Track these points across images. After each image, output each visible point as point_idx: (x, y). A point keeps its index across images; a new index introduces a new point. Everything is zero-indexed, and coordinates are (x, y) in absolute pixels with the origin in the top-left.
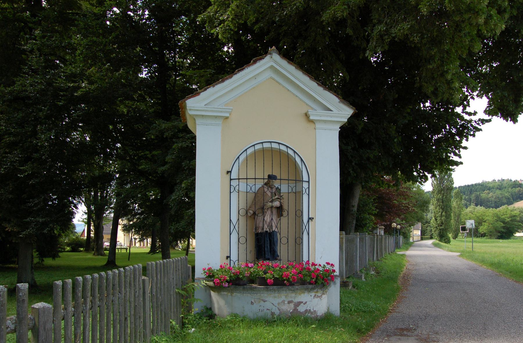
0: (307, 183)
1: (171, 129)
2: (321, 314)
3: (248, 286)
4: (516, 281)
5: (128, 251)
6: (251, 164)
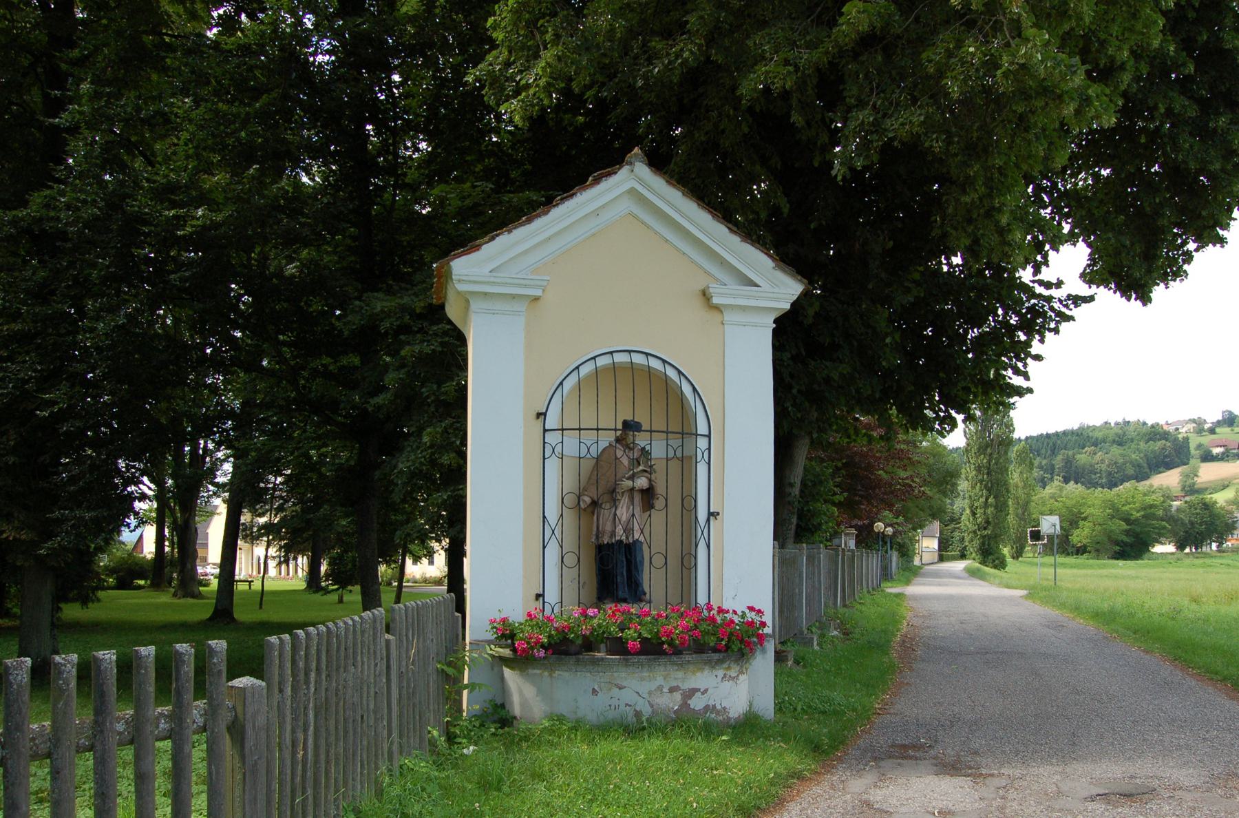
0: (706, 439)
2: (736, 716)
3: (586, 656)
4: (1146, 652)
6: (589, 396)
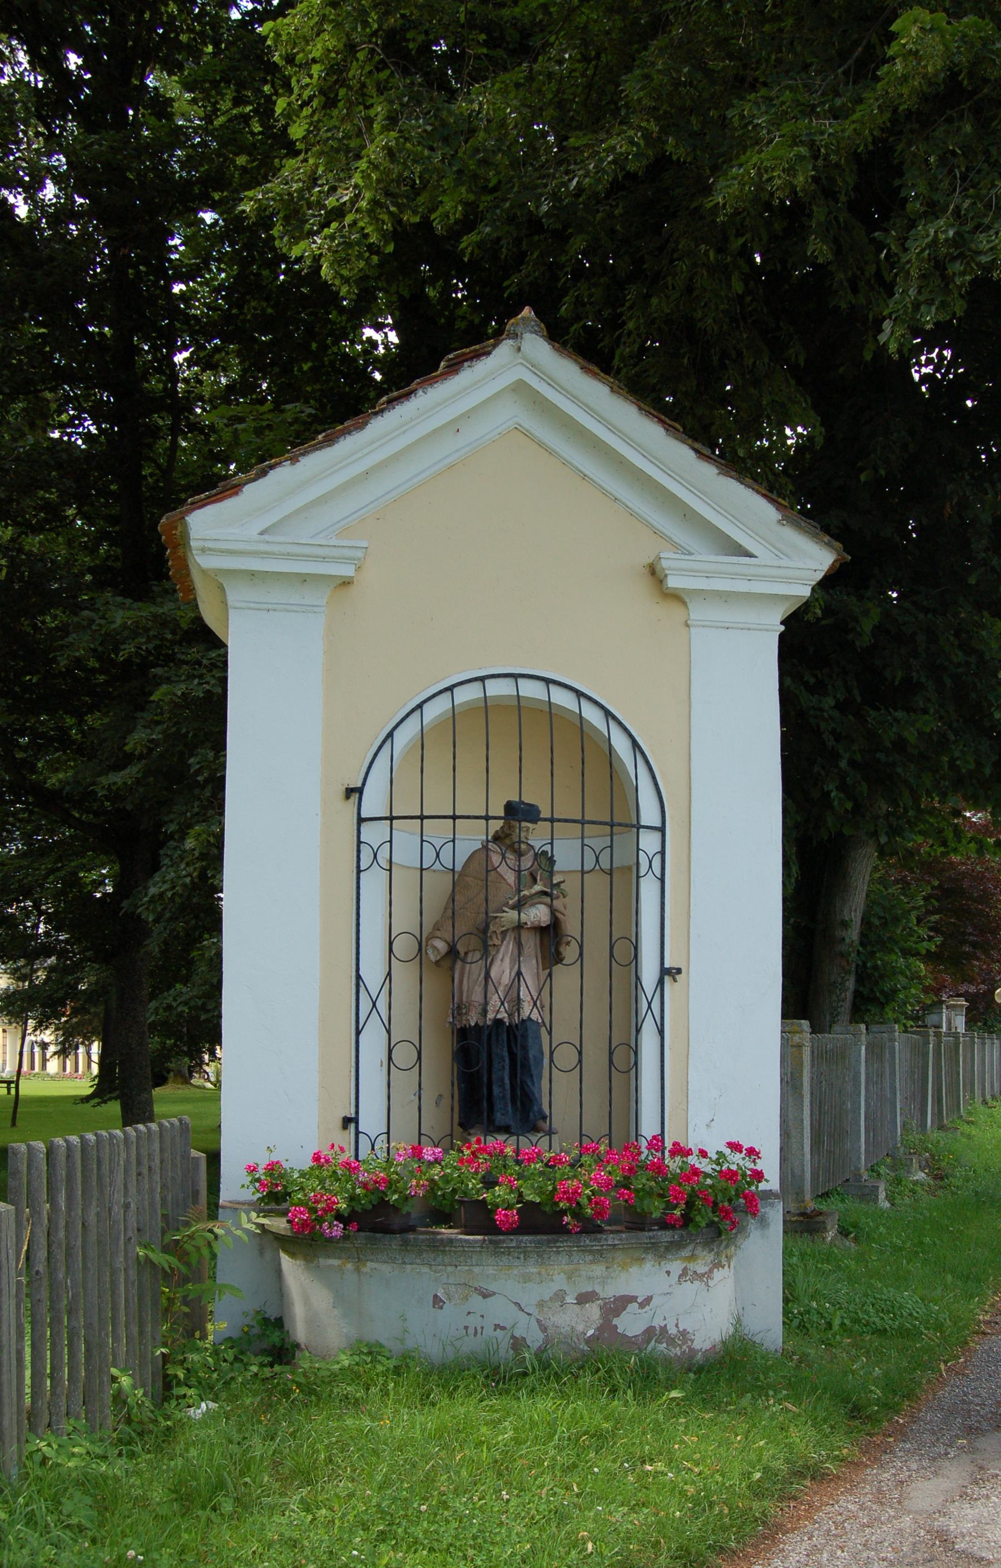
0: (657, 835)
1: (147, 630)
2: (707, 1345)
5: (13, 1091)
